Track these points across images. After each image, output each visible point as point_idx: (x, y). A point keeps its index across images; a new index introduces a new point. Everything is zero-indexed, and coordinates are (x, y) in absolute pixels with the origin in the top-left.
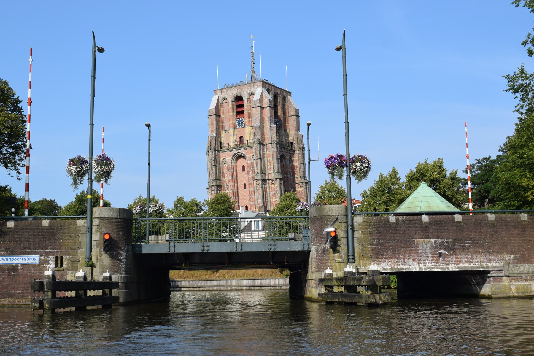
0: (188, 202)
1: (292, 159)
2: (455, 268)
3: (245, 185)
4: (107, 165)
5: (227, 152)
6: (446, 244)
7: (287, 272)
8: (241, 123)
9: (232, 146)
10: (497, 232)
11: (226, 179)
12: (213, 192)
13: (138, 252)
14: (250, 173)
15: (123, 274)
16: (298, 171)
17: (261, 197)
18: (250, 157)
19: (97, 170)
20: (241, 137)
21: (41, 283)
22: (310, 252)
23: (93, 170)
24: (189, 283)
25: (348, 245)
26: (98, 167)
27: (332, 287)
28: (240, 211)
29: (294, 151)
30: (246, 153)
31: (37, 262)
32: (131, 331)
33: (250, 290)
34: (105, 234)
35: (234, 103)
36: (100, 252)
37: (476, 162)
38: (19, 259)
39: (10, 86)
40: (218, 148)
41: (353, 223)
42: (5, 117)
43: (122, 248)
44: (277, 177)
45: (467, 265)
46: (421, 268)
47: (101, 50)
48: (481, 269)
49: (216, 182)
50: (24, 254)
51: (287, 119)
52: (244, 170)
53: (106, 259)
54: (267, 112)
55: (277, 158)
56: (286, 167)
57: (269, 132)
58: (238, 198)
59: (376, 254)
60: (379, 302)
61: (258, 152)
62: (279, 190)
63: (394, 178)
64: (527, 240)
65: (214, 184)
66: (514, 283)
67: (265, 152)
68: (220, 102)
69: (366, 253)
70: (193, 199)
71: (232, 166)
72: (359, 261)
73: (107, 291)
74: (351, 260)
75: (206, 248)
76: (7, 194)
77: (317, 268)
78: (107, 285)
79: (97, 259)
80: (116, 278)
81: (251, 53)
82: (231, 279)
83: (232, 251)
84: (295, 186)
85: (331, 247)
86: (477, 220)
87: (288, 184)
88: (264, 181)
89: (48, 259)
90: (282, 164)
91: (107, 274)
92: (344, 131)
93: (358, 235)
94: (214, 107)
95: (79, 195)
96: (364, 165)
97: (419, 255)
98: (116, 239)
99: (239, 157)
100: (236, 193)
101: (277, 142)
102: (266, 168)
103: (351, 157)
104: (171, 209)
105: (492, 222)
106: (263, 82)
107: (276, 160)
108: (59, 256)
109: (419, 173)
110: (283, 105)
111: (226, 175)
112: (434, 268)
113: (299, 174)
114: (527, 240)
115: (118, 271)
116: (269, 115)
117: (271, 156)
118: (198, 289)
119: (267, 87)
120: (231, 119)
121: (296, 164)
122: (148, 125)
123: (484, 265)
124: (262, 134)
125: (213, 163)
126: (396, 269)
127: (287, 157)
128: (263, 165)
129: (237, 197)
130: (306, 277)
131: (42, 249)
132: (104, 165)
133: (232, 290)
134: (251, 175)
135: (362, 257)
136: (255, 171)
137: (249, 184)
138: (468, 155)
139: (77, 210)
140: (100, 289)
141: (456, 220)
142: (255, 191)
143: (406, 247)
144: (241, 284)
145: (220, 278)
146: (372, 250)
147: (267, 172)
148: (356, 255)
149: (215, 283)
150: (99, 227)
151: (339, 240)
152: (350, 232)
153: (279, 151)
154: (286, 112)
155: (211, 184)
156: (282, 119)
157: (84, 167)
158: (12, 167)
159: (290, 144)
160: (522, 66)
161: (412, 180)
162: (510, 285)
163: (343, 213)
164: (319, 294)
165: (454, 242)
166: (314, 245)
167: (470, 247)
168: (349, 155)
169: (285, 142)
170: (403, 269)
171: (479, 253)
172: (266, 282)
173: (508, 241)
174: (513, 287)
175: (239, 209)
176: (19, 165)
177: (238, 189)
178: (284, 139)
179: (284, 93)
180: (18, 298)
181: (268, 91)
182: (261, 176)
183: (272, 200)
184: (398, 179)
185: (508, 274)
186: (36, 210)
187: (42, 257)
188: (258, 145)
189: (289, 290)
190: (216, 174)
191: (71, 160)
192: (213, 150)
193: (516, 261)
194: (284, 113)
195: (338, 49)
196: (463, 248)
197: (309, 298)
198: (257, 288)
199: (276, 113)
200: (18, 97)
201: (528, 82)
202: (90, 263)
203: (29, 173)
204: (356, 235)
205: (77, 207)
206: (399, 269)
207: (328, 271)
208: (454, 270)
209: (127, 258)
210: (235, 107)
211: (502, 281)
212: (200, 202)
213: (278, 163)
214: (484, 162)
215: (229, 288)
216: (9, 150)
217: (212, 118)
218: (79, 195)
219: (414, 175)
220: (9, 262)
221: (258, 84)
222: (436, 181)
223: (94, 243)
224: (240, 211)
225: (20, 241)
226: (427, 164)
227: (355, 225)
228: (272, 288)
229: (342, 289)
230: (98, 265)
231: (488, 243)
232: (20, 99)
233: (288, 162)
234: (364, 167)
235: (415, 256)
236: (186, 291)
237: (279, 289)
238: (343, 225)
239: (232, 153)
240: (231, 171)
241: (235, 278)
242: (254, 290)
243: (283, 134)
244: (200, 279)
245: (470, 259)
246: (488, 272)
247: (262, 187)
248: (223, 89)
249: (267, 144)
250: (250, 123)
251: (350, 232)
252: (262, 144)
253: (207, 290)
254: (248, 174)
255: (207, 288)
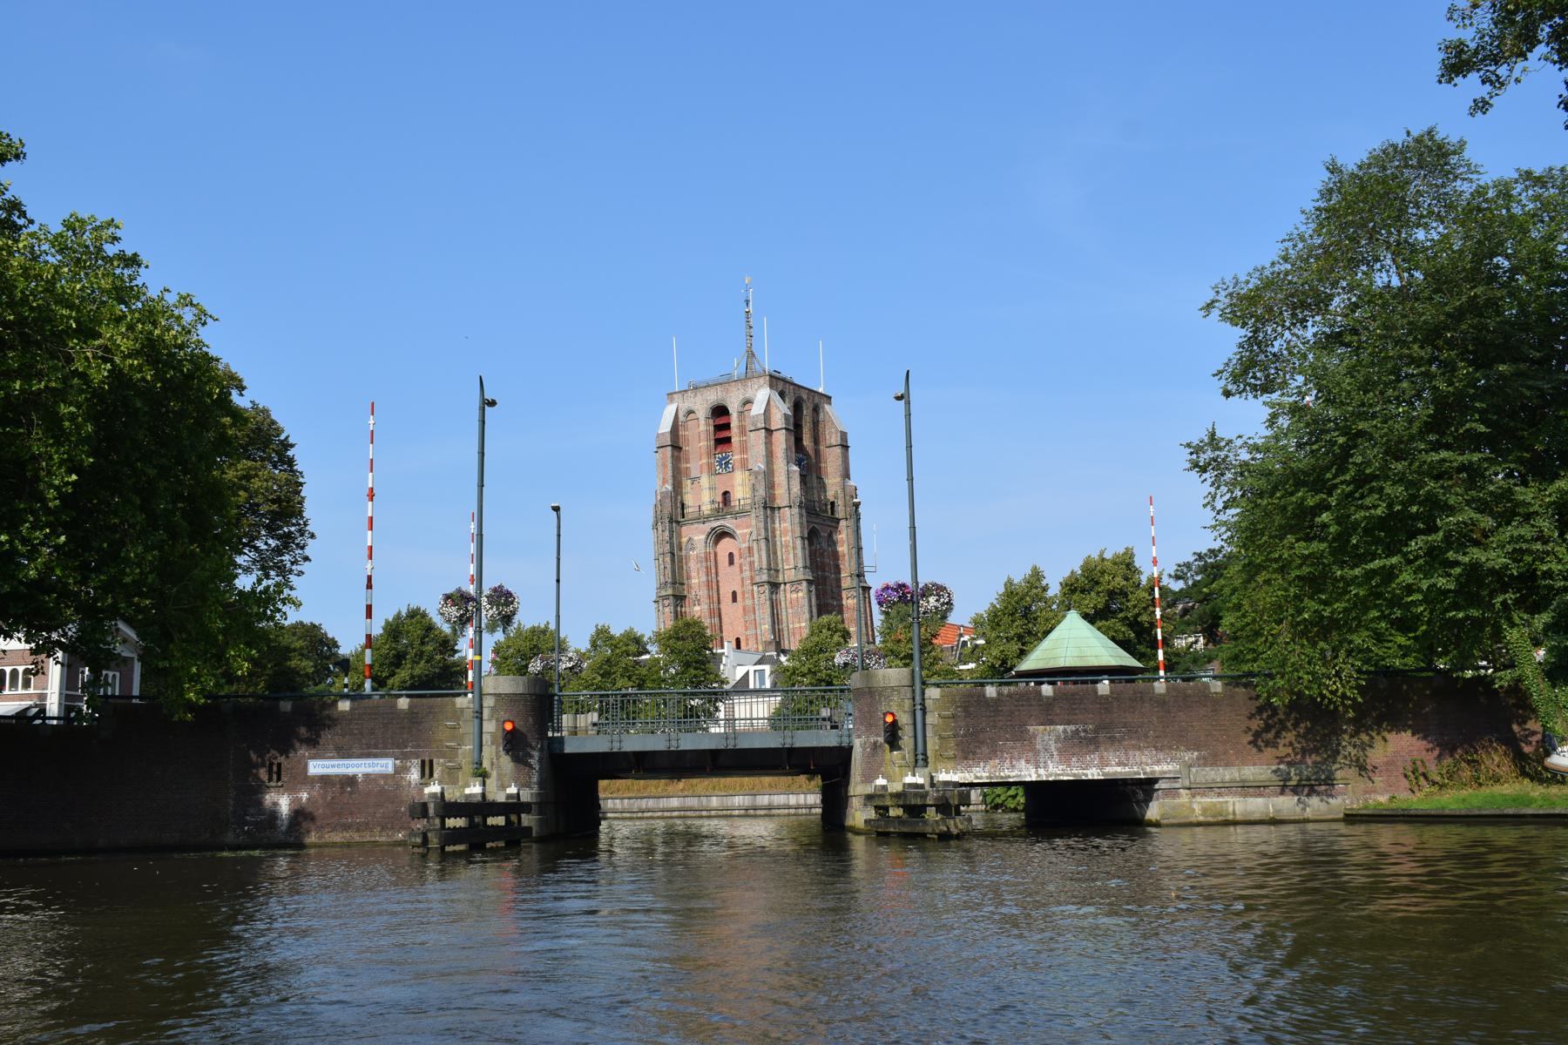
0: (618, 635)
1: (835, 537)
2: (1099, 775)
3: (734, 594)
4: (507, 604)
5: (696, 525)
6: (1082, 734)
7: (818, 781)
8: (725, 463)
9: (706, 512)
10: (1169, 712)
11: (694, 581)
12: (667, 610)
13: (557, 751)
14: (744, 568)
15: (535, 790)
16: (847, 564)
17: (768, 619)
18: (745, 534)
19: (491, 612)
20: (726, 494)
21: (424, 806)
22: (852, 747)
23: (484, 613)
24: (622, 804)
25: (915, 737)
26: (491, 608)
27: (886, 809)
28: (725, 651)
29: (838, 521)
30: (737, 527)
31: (390, 770)
33: (747, 816)
34: (504, 722)
35: (711, 421)
36: (497, 753)
37: (1194, 558)
38: (358, 766)
39: (274, 417)
40: (676, 517)
41: (924, 699)
42: (266, 481)
43: (534, 744)
44: (801, 577)
45: (1119, 769)
46: (1039, 776)
47: (492, 403)
48: (1142, 776)
49: (674, 588)
50: (368, 756)
51: (822, 453)
52: (731, 562)
53: (506, 762)
54: (781, 440)
55: (803, 538)
56: (822, 555)
57: (785, 483)
58: (721, 622)
59: (963, 751)
60: (955, 831)
61: (762, 525)
62: (806, 604)
63: (1036, 588)
64: (1221, 725)
65: (670, 592)
66: (1198, 799)
67: (777, 525)
68: (681, 418)
69: (946, 751)
70: (628, 629)
71: (707, 555)
72: (935, 763)
73: (514, 818)
74: (920, 762)
75: (674, 743)
77: (864, 776)
78: (513, 807)
79: (492, 764)
80: (526, 796)
81: (744, 315)
82: (707, 794)
83: (719, 748)
84: (841, 596)
85: (887, 741)
86: (1135, 693)
87: (825, 592)
88: (775, 586)
89: (409, 764)
90: (813, 548)
91: (513, 790)
92: (908, 543)
93: (931, 719)
94: (669, 430)
95: (390, 620)
96: (942, 600)
97: (1036, 753)
98: (524, 730)
99: (721, 535)
100: (716, 611)
101: (801, 502)
102: (780, 558)
103: (921, 586)
104: (583, 651)
105: (1160, 695)
106: (771, 376)
107: (799, 542)
108: (427, 759)
109: (1087, 578)
110: (814, 423)
111: (694, 574)
112: (1062, 775)
113: (848, 570)
114: (1221, 725)
115: (528, 785)
116: (784, 446)
117: (790, 534)
118: (640, 815)
119: (781, 386)
120: (705, 456)
121: (843, 549)
122: (556, 509)
123: (1148, 769)
124: (770, 486)
125: (668, 547)
126: (997, 777)
127: (822, 534)
128: (772, 552)
129: (717, 619)
130: (847, 791)
131: (398, 748)
132: (503, 605)
133: (709, 817)
134: (747, 574)
135: (940, 757)
136: (756, 564)
137: (743, 593)
138: (1155, 558)
139: (388, 654)
140: (501, 815)
141: (1100, 693)
142: (756, 608)
143: (1015, 739)
144: (729, 804)
145: (686, 793)
146: (957, 745)
147: (780, 566)
148: (929, 753)
149: (675, 803)
150: (493, 709)
151: (900, 729)
152: (919, 714)
153: (805, 523)
154: (821, 439)
155: (663, 593)
156: (811, 453)
157: (470, 608)
158: (277, 576)
159: (829, 507)
160: (1213, 429)
161: (1073, 591)
162: (1191, 802)
163: (906, 682)
164: (866, 821)
165: (1096, 731)
166: (859, 737)
167: (1123, 738)
168: (917, 583)
169: (820, 501)
170: (1009, 777)
171: (1139, 749)
172: (779, 799)
173: (1190, 729)
174: (1196, 806)
175: (722, 647)
176: (291, 571)
177: (719, 603)
178: (816, 496)
179: (816, 398)
180: (358, 830)
181: (782, 395)
182: (769, 576)
183: (791, 626)
184: (1045, 589)
185: (1187, 784)
186: (295, 650)
187: (398, 762)
188: (762, 509)
189: (823, 815)
190: (673, 572)
191: (447, 597)
192: (667, 520)
193: (1202, 761)
194: (816, 440)
195: (899, 398)
196: (1112, 740)
197: (851, 827)
198: (762, 812)
199: (798, 440)
200: (287, 437)
201: (1223, 454)
202: (480, 771)
203: (371, 618)
204: (929, 720)
205: (388, 646)
206: (1002, 777)
207: (881, 781)
208: (1096, 778)
209: (540, 761)
210: (712, 428)
211: (1178, 795)
212: (643, 636)
213: (804, 548)
214: (1210, 558)
215: (704, 813)
216: (270, 541)
217: (663, 453)
218: (390, 620)
219: (1077, 580)
221: (761, 380)
222: (1120, 594)
223: (486, 738)
224: (725, 651)
225: (361, 734)
226: (1103, 560)
227: (928, 703)
228: (792, 811)
229: (900, 812)
230: (494, 774)
231: (1154, 731)
232: (291, 441)
233: (824, 545)
234: (943, 604)
235: (1030, 754)
236: (615, 818)
237: (806, 815)
238: (907, 704)
239: (708, 526)
240: (704, 564)
241: (717, 792)
242: (755, 816)
243: (815, 485)
244: (645, 795)
245: (1123, 759)
246: (1155, 781)
247: (771, 600)
248: (686, 391)
249: (779, 508)
250: (744, 465)
251: (919, 714)
252: (770, 507)
253: (658, 818)
254: (741, 571)
255: (659, 814)
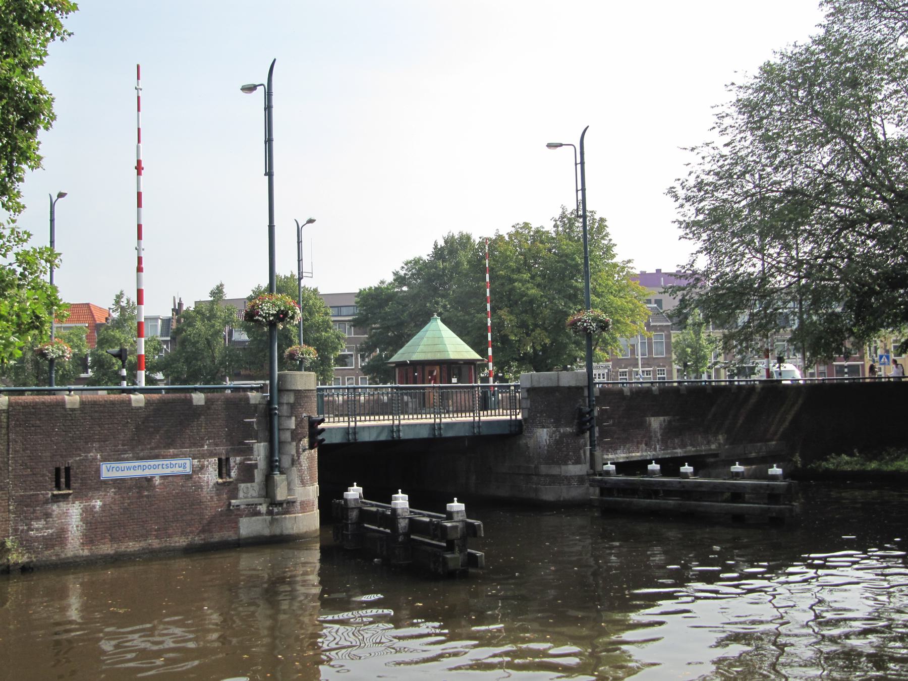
32: (681, 579)
76: (464, 257)
220: (139, 473)
